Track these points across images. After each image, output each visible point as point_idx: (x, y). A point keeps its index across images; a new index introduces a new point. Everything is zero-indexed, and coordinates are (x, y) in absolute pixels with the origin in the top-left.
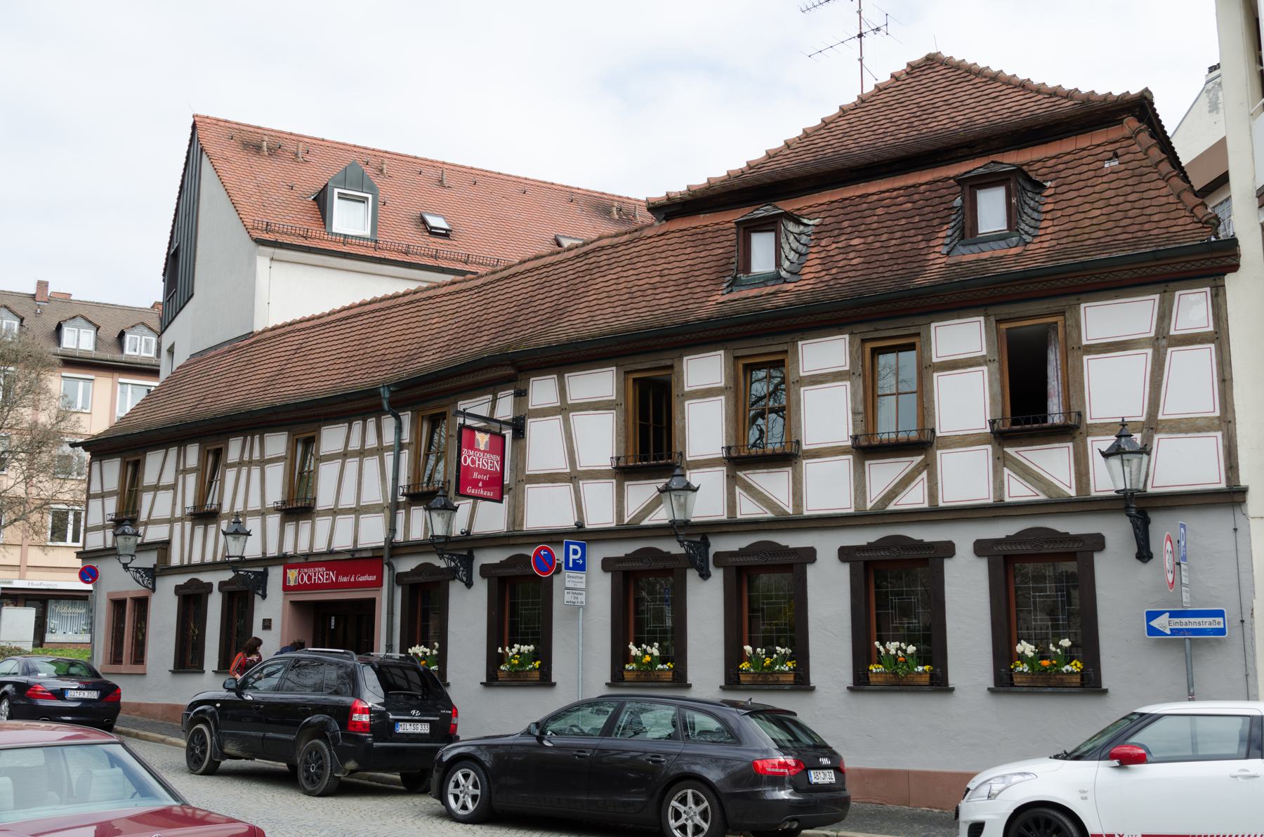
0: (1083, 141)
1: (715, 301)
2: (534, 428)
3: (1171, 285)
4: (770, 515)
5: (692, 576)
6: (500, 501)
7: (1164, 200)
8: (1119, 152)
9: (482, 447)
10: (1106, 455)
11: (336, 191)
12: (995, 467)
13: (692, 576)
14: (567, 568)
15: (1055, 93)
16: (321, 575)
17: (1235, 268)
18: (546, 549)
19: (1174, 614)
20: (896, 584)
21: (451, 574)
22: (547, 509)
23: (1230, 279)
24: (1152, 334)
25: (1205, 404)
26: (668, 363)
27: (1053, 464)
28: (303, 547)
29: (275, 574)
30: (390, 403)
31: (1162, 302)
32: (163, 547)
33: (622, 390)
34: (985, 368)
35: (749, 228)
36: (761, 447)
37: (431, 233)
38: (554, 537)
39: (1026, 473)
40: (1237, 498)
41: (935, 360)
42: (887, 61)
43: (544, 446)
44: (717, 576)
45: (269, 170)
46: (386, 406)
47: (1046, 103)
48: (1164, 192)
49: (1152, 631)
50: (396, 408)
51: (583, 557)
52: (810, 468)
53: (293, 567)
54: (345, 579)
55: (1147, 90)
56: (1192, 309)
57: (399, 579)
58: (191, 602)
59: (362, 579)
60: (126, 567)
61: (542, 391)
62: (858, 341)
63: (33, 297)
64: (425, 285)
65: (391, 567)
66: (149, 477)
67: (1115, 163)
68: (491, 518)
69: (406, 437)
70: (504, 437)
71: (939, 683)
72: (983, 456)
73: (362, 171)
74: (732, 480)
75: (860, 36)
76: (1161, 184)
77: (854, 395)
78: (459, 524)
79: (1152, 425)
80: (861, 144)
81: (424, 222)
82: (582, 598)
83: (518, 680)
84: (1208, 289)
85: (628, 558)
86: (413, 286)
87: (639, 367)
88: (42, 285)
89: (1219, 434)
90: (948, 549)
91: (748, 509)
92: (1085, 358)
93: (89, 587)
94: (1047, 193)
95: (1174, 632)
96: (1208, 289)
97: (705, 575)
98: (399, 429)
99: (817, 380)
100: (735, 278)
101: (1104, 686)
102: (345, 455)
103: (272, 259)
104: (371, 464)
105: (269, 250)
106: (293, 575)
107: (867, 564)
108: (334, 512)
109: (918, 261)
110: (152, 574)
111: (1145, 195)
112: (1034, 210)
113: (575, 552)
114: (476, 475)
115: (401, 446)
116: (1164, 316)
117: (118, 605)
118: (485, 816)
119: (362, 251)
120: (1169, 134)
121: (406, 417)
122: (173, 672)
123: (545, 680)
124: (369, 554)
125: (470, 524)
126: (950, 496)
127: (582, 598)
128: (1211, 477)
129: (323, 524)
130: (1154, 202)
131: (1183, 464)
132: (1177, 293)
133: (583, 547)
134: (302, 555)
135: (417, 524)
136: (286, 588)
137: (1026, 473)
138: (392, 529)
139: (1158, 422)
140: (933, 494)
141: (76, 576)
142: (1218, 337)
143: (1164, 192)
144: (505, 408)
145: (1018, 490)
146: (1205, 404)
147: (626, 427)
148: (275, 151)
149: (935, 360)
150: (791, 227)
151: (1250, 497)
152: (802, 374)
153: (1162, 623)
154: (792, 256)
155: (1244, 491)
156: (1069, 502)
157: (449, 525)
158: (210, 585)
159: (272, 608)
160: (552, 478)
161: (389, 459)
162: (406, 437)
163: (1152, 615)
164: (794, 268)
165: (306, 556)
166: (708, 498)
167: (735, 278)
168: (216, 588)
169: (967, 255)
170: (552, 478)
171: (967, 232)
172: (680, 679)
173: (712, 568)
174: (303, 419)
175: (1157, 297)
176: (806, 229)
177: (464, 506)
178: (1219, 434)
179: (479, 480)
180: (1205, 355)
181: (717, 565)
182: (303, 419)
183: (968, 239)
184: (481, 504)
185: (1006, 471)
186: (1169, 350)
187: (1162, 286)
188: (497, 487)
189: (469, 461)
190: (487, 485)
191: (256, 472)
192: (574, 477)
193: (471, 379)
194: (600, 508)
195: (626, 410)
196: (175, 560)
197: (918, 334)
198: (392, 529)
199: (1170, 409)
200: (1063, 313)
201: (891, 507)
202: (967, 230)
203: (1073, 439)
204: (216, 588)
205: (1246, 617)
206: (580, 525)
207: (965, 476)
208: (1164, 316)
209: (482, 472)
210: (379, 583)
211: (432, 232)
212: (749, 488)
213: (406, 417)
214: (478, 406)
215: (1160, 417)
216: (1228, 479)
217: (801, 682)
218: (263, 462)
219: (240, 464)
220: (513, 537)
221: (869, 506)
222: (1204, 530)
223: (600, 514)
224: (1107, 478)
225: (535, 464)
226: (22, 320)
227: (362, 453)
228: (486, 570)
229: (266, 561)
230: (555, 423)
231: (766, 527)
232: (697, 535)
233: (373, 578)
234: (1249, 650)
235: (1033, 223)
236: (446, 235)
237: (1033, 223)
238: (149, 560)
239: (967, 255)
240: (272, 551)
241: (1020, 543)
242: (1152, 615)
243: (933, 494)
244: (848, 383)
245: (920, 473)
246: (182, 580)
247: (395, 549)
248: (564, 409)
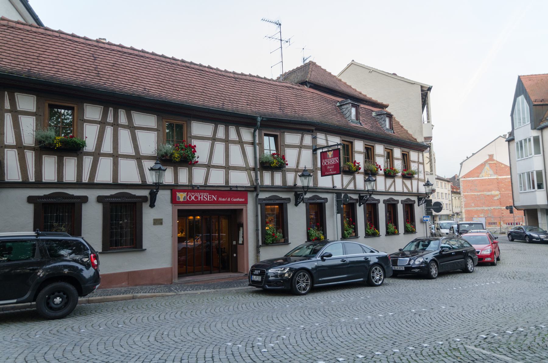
9: (330, 157)
10: (300, 176)
54: (224, 200)
58: (391, 207)
59: (235, 200)
71: (356, 236)
83: (275, 243)
90: (85, 199)
107: (44, 204)
120: (530, 125)
123: (286, 242)
140: (355, 186)
158: (379, 201)
168: (381, 202)
184: (334, 176)
193: (298, 127)
204: (381, 202)
206: (295, 185)
209: (330, 165)
210: (246, 203)
243: (355, 186)
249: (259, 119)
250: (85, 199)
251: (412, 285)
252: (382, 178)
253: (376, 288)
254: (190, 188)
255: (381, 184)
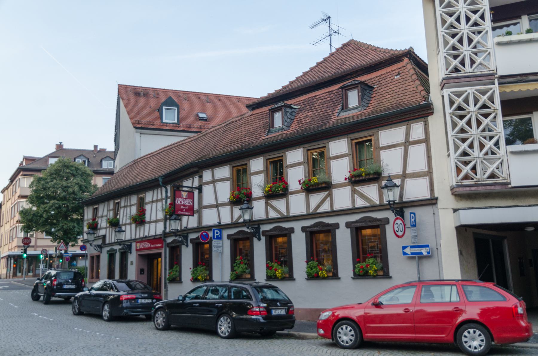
0: (389, 69)
1: (264, 138)
2: (205, 188)
3: (410, 122)
4: (279, 216)
5: (255, 240)
6: (193, 216)
7: (412, 89)
8: (400, 72)
9: (184, 197)
11: (164, 107)
12: (352, 194)
13: (255, 240)
14: (214, 238)
15: (385, 51)
16: (146, 245)
17: (432, 113)
18: (205, 232)
19: (412, 247)
20: (320, 239)
21: (182, 243)
22: (210, 218)
23: (430, 118)
24: (404, 141)
25: (423, 167)
26: (245, 163)
27: (371, 192)
28: (142, 235)
29: (134, 245)
30: (163, 183)
31: (407, 129)
32: (104, 237)
33: (232, 174)
34: (347, 158)
35: (274, 111)
36: (277, 190)
37: (200, 120)
38: (210, 228)
39: (363, 196)
40: (434, 201)
41: (331, 156)
42: (338, 42)
43: (208, 196)
44: (263, 239)
45: (143, 102)
46: (161, 184)
47: (381, 55)
48: (412, 86)
49: (405, 254)
50: (165, 184)
51: (221, 234)
52: (292, 198)
53: (138, 242)
55: (411, 48)
56: (417, 130)
57: (168, 245)
58: (111, 256)
60: (91, 245)
61: (207, 175)
62: (306, 150)
63: (93, 151)
64: (186, 138)
65: (166, 241)
66: (100, 213)
67: (398, 77)
68: (191, 222)
69: (169, 195)
70: (194, 193)
71: (335, 276)
72: (348, 190)
73: (171, 99)
74: (267, 204)
75: (330, 35)
76: (412, 83)
77: (305, 171)
78: (184, 225)
79: (404, 176)
80: (316, 78)
81: (198, 116)
82: (221, 249)
84: (422, 123)
85: (235, 234)
86: (183, 138)
87: (237, 165)
88: (96, 147)
89: (428, 178)
90: (337, 226)
91: (273, 214)
92: (381, 151)
93: (84, 252)
94: (376, 89)
95: (412, 254)
96: (422, 123)
97: (259, 239)
98: (167, 192)
99: (293, 166)
100: (269, 130)
101: (390, 275)
102: (152, 202)
103: (141, 134)
104: (159, 204)
105: (140, 130)
106: (138, 245)
108: (150, 222)
109: (328, 118)
110: (100, 247)
111: (406, 88)
112: (369, 97)
113: (217, 233)
114: (182, 207)
115: (167, 197)
116: (408, 134)
117: (92, 258)
118: (167, 328)
119: (173, 128)
121: (169, 187)
122: (353, 278)
124: (153, 238)
125: (187, 225)
126: (338, 206)
127: (221, 249)
128: (425, 195)
129: (147, 226)
130: (408, 91)
131: (416, 190)
132: (412, 125)
133: (220, 231)
134: (153, 236)
135: (174, 226)
136: (137, 250)
137: (363, 196)
138: (165, 228)
139: (406, 174)
141: (79, 248)
142: (426, 140)
143: (412, 86)
144: (196, 184)
145: (360, 203)
146: (423, 167)
147: (233, 187)
148: (145, 95)
149: (331, 156)
150: (288, 110)
151: (439, 202)
152: (288, 164)
153: (408, 251)
154: (288, 120)
155: (436, 199)
156: (377, 206)
157: (181, 226)
159: (133, 257)
160: (211, 207)
161: (164, 201)
162: (169, 195)
163: (404, 248)
164: (289, 125)
165: (142, 238)
166: (259, 210)
167: (269, 130)
168: (342, 225)
169: (344, 115)
170: (211, 207)
171: (344, 107)
172: (252, 278)
173: (261, 237)
174: (140, 188)
175: (405, 127)
176: (295, 110)
177: (185, 219)
178: (428, 178)
179: (183, 209)
180: (422, 147)
181: (263, 235)
182: (140, 188)
183: (345, 110)
185: (356, 195)
186: (410, 146)
187: (407, 123)
188: (191, 211)
189: (179, 202)
190: (187, 210)
191: (129, 209)
192: (217, 206)
194: (226, 215)
195: (233, 181)
196: (107, 242)
197: (325, 147)
198: (165, 228)
199: (410, 169)
200: (373, 135)
201: (318, 211)
202: (345, 107)
203: (378, 182)
204: (342, 225)
205: (439, 247)
206: (219, 223)
207: (342, 198)
208: (408, 134)
209: (184, 206)
211: (201, 119)
212: (272, 207)
213: (169, 187)
214: (187, 183)
215: (407, 172)
216: (431, 194)
217: (290, 277)
218: (131, 206)
219: (125, 207)
220: (199, 228)
221: (311, 211)
222: (422, 213)
223: (226, 220)
224: (392, 196)
225: (205, 202)
226: (88, 159)
227: (157, 201)
228: (192, 240)
229: (132, 240)
230: (211, 186)
231: (278, 220)
232: (255, 224)
233: (160, 245)
234: (440, 259)
235: (367, 102)
236: (206, 120)
237: (367, 102)
238: (100, 242)
239: (344, 115)
240: (133, 237)
241: (360, 222)
242: (404, 248)
244: (303, 166)
245: (327, 198)
246: (108, 249)
247: (166, 234)
248: (214, 182)
249: (161, 180)
250: (337, 226)
251: (183, 339)
252: (302, 196)
253: (219, 339)
254: (140, 240)
255: (297, 204)
